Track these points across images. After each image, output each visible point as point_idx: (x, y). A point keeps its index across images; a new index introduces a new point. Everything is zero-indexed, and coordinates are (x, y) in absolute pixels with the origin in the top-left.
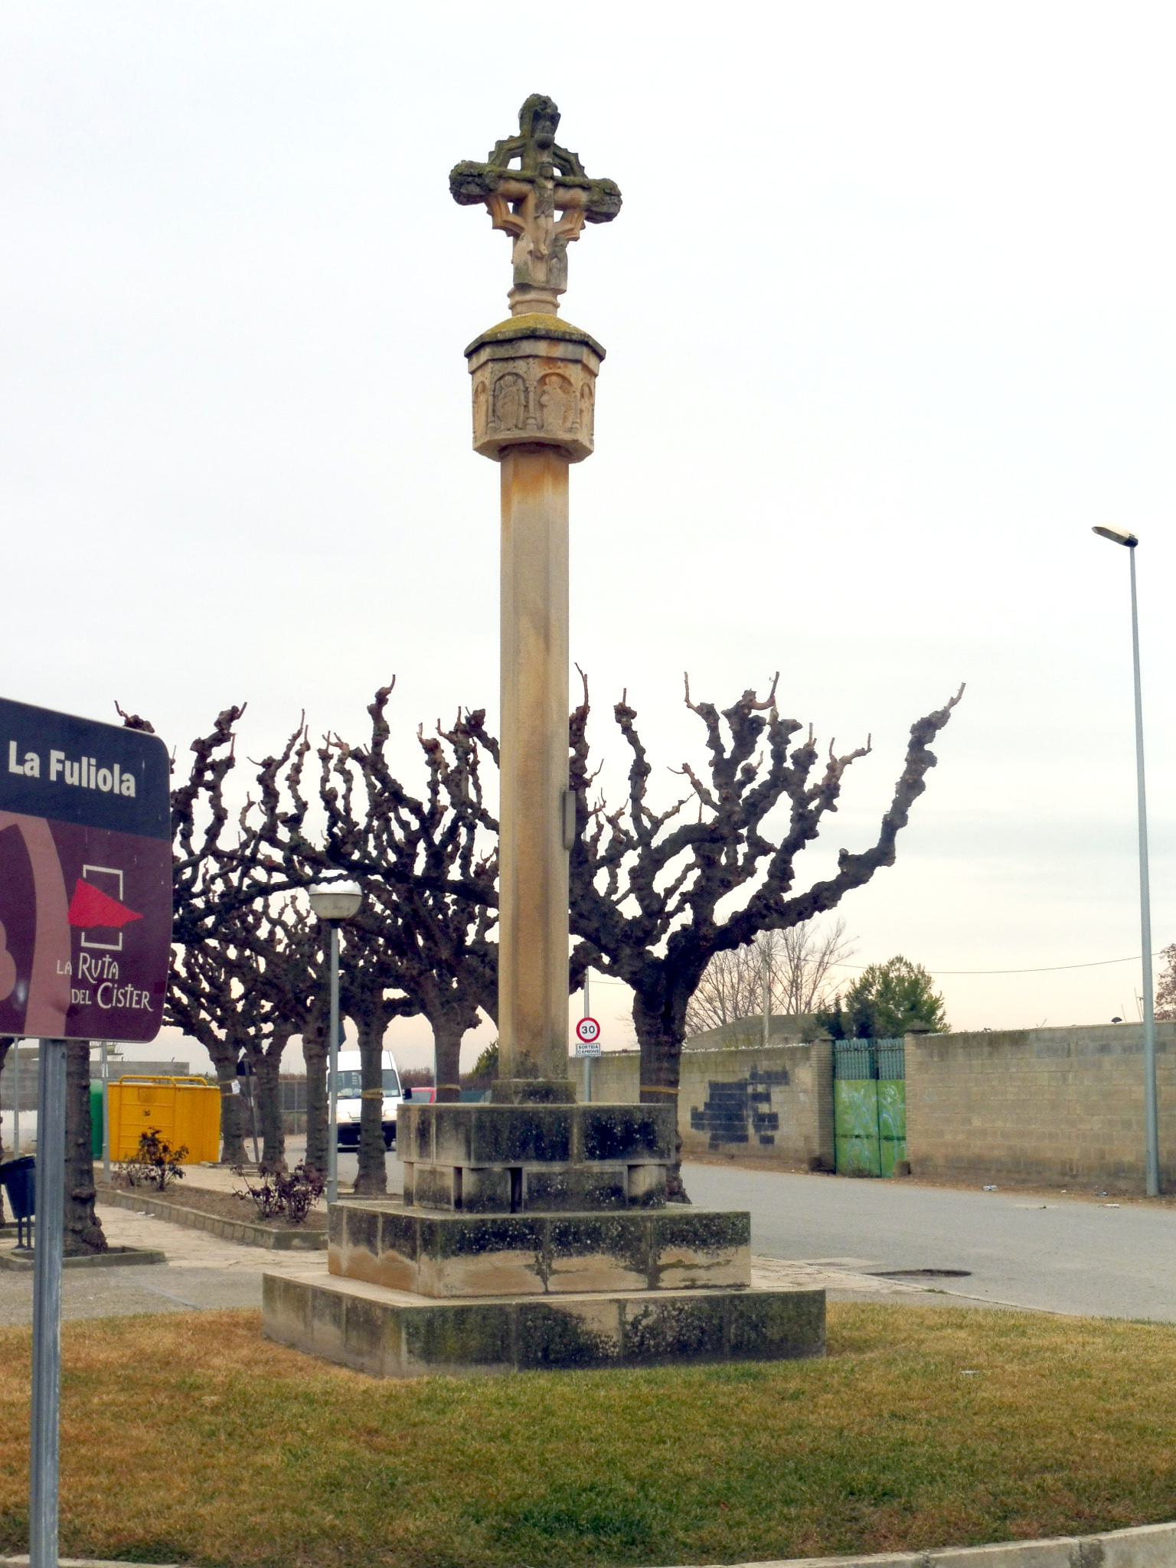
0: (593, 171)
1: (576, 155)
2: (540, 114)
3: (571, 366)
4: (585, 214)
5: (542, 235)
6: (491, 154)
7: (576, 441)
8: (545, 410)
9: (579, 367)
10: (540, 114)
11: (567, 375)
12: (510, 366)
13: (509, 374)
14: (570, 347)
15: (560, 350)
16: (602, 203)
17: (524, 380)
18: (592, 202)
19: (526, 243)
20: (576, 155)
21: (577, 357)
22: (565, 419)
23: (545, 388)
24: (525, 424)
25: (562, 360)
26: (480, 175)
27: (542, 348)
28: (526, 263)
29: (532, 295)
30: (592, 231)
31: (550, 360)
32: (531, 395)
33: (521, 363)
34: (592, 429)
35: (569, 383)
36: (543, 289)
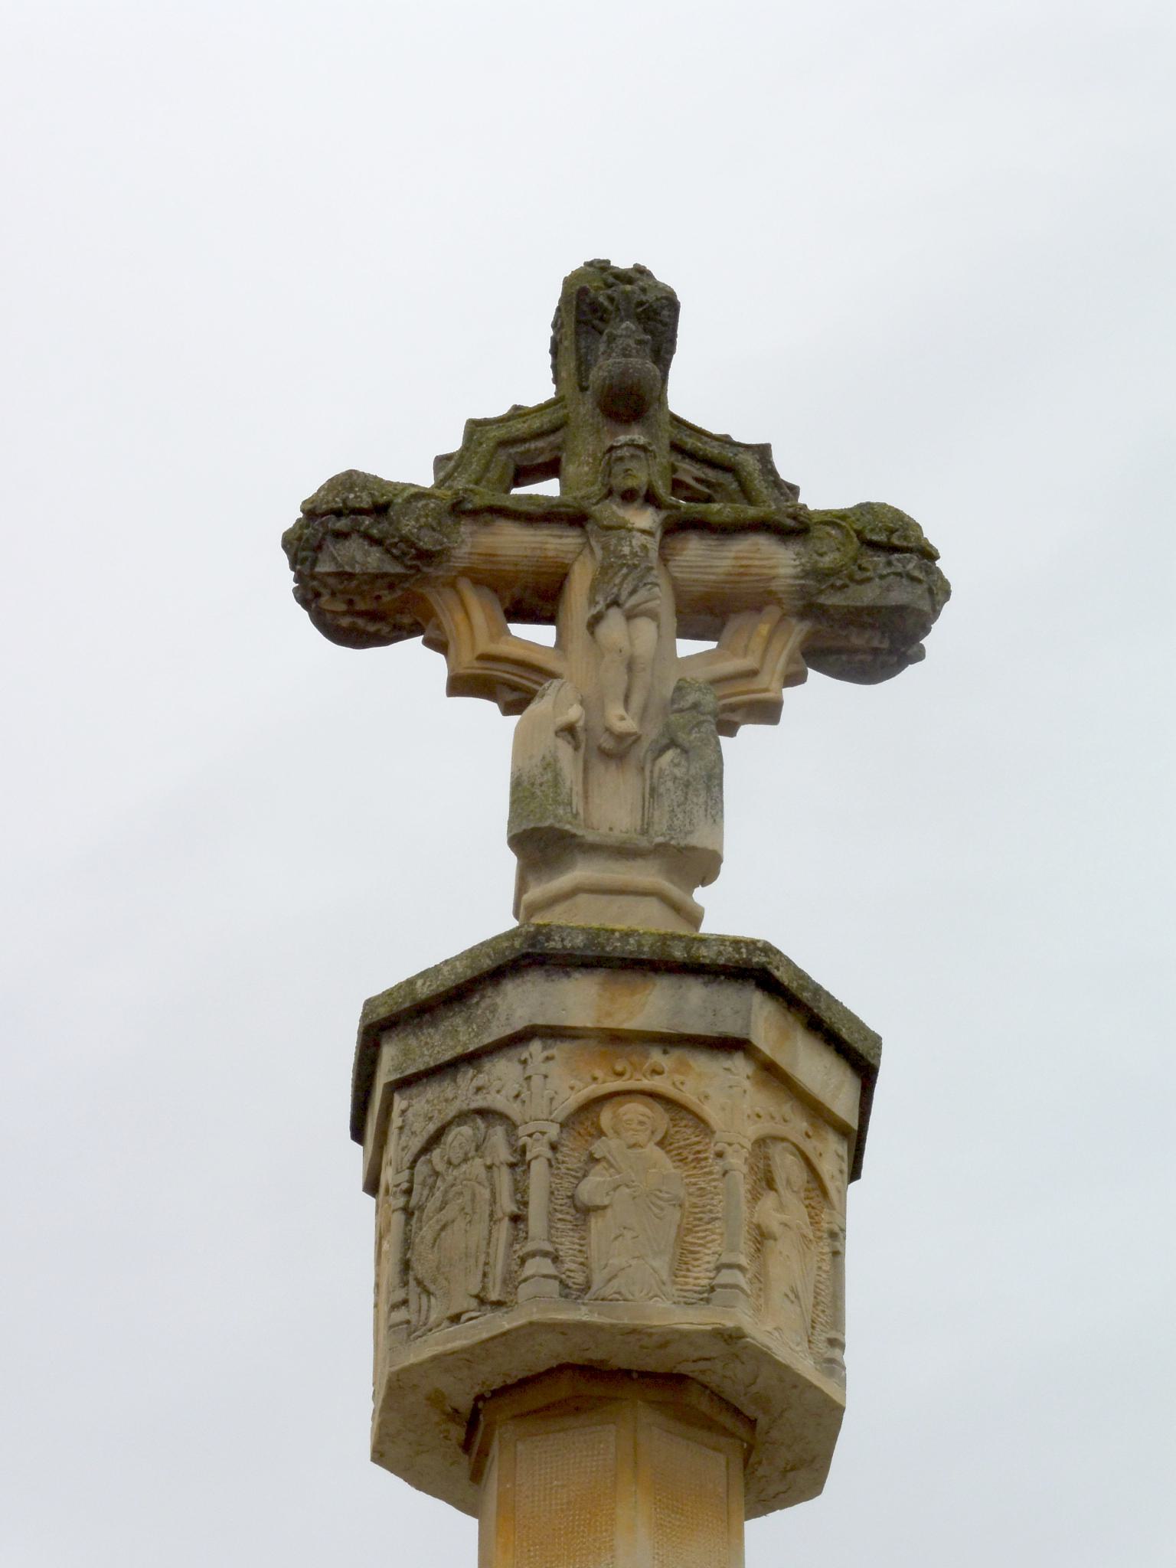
0: (824, 480)
1: (763, 452)
2: (615, 321)
3: (703, 1063)
4: (798, 631)
5: (616, 677)
6: (441, 461)
7: (731, 1338)
8: (596, 1223)
9: (740, 1066)
10: (615, 321)
11: (688, 1094)
12: (462, 1092)
13: (462, 1117)
14: (696, 994)
15: (654, 1005)
16: (867, 598)
17: (511, 1126)
18: (821, 575)
19: (555, 705)
20: (763, 452)
21: (730, 1027)
22: (683, 1257)
23: (599, 1148)
24: (511, 1281)
25: (669, 1041)
26: (380, 510)
27: (577, 1000)
28: (550, 765)
29: (581, 872)
30: (818, 698)
31: (617, 1040)
32: (538, 1175)
33: (503, 1070)
34: (837, 1320)
35: (701, 1123)
36: (624, 852)
